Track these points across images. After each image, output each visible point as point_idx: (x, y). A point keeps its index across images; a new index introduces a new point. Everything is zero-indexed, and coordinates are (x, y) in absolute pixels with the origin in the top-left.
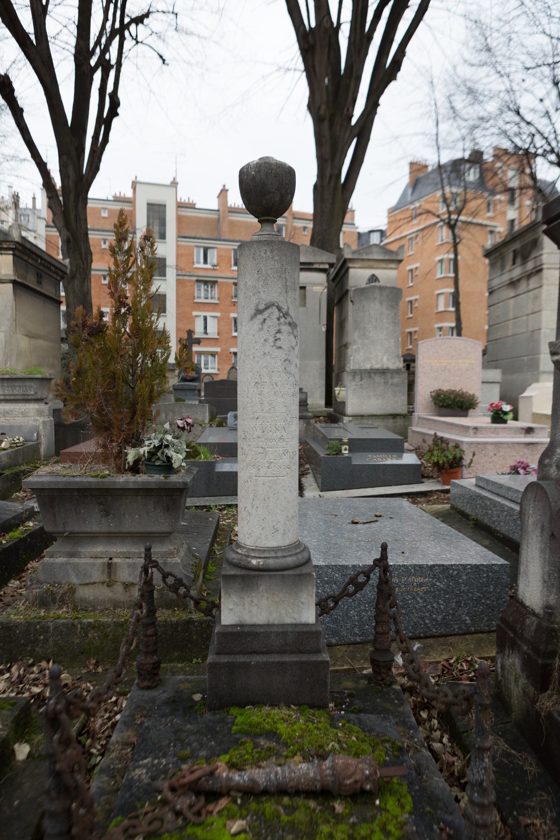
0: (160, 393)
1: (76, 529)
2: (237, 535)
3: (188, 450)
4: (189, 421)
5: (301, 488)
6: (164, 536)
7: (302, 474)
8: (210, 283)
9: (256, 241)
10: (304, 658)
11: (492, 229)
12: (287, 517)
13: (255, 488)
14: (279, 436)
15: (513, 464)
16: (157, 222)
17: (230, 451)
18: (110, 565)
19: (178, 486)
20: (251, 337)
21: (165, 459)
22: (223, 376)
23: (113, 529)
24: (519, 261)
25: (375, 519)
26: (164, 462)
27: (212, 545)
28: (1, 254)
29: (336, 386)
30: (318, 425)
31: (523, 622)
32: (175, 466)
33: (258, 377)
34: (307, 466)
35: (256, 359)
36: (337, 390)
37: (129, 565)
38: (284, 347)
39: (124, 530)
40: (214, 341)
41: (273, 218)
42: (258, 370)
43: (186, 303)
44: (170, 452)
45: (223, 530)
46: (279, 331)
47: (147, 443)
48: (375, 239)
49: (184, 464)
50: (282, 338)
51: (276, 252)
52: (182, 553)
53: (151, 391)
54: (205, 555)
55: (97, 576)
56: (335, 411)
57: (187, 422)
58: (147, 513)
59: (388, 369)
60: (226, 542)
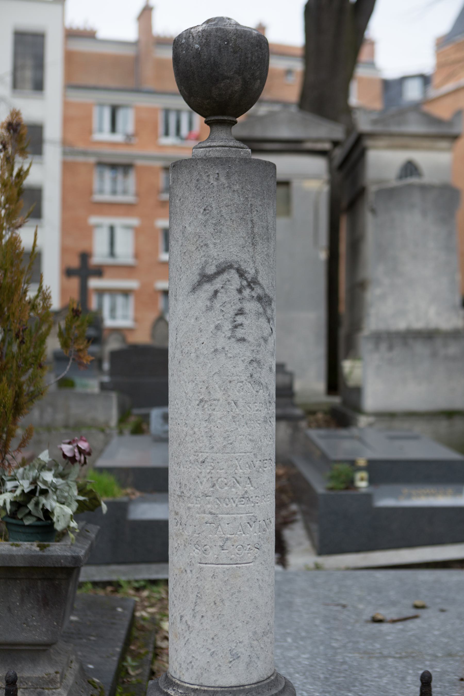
0: (33, 396)
2: (167, 638)
3: (81, 498)
4: (84, 445)
5: (281, 548)
6: (37, 651)
7: (282, 524)
8: (122, 167)
9: (202, 159)
12: (255, 633)
13: (199, 584)
14: (240, 493)
16: (29, 62)
17: (155, 481)
19: (64, 563)
20: (193, 320)
21: (41, 515)
22: (142, 337)
25: (413, 612)
26: (39, 519)
27: (122, 658)
29: (347, 357)
30: (314, 433)
32: (59, 526)
33: (203, 390)
34: (294, 507)
35: (202, 358)
36: (347, 365)
38: (250, 339)
40: (127, 270)
41: (231, 118)
42: (205, 378)
43: (79, 203)
44: (50, 503)
45: (142, 629)
46: (241, 312)
47: (9, 485)
48: (413, 92)
49: (74, 524)
50: (246, 322)
51: (235, 177)
52: (70, 680)
53: (18, 395)
54: (110, 678)
56: (345, 403)
57: (79, 448)
58: (9, 610)
60: (147, 653)
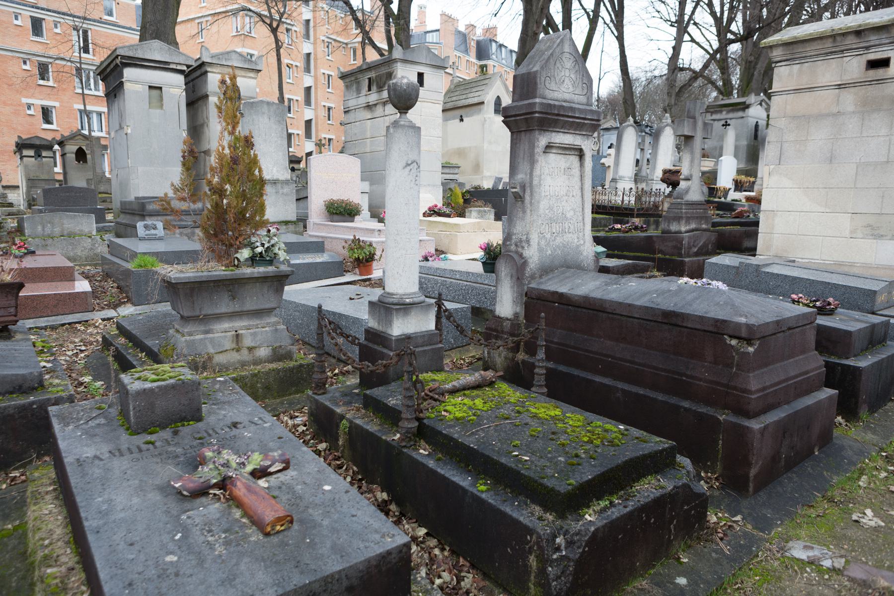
1: (210, 312)
10: (433, 347)
11: (289, 27)
15: (424, 254)
18: (237, 336)
23: (237, 310)
24: (374, 88)
28: (890, 268)
31: (502, 325)
37: (252, 334)
39: (245, 309)
55: (228, 345)
59: (278, 180)
